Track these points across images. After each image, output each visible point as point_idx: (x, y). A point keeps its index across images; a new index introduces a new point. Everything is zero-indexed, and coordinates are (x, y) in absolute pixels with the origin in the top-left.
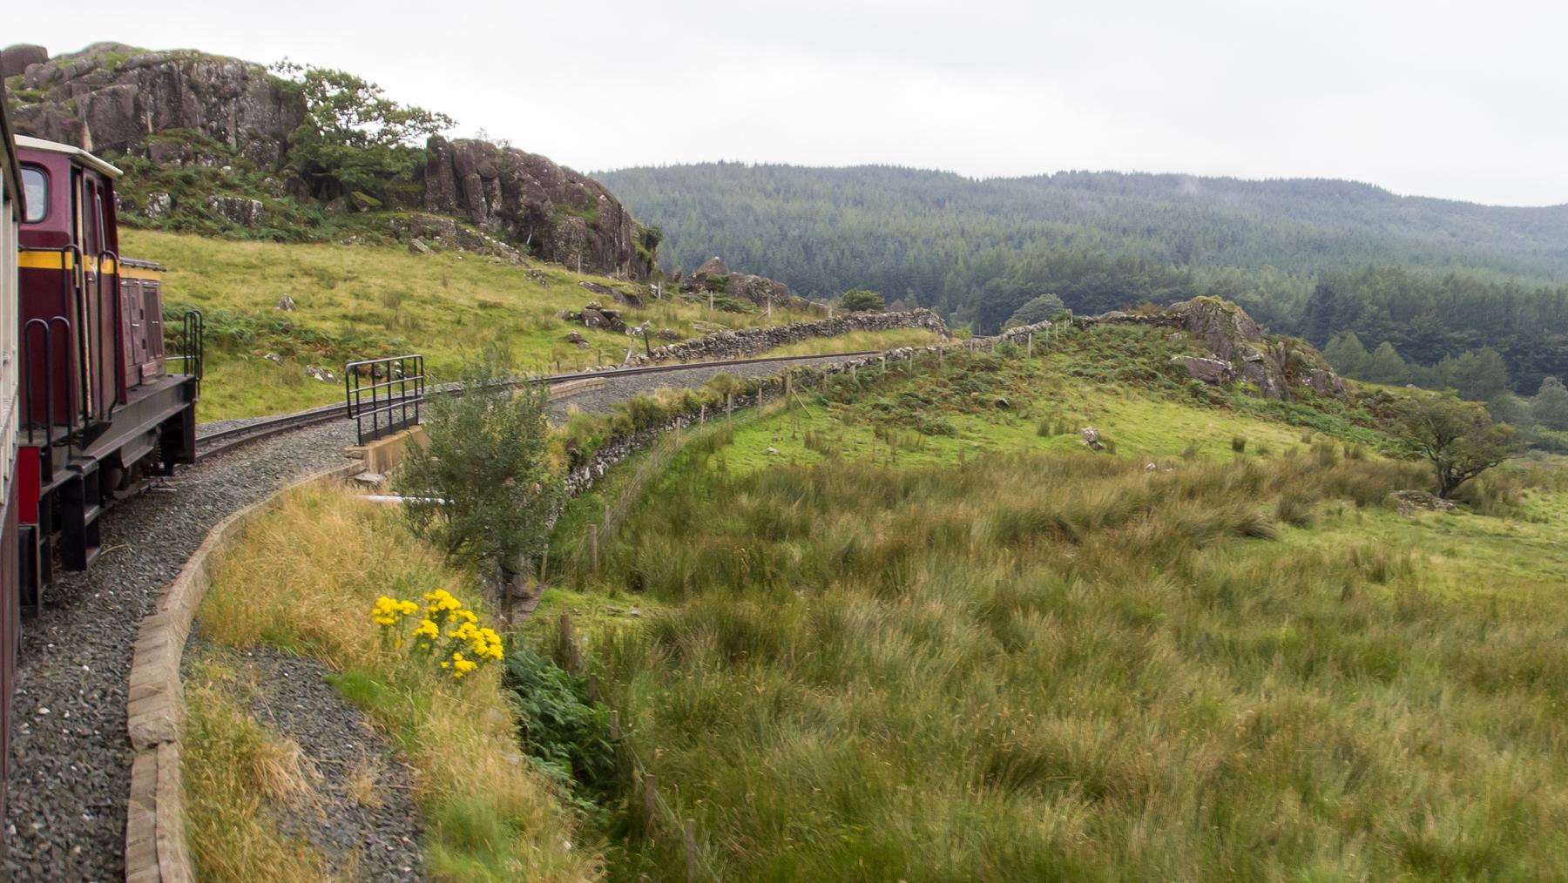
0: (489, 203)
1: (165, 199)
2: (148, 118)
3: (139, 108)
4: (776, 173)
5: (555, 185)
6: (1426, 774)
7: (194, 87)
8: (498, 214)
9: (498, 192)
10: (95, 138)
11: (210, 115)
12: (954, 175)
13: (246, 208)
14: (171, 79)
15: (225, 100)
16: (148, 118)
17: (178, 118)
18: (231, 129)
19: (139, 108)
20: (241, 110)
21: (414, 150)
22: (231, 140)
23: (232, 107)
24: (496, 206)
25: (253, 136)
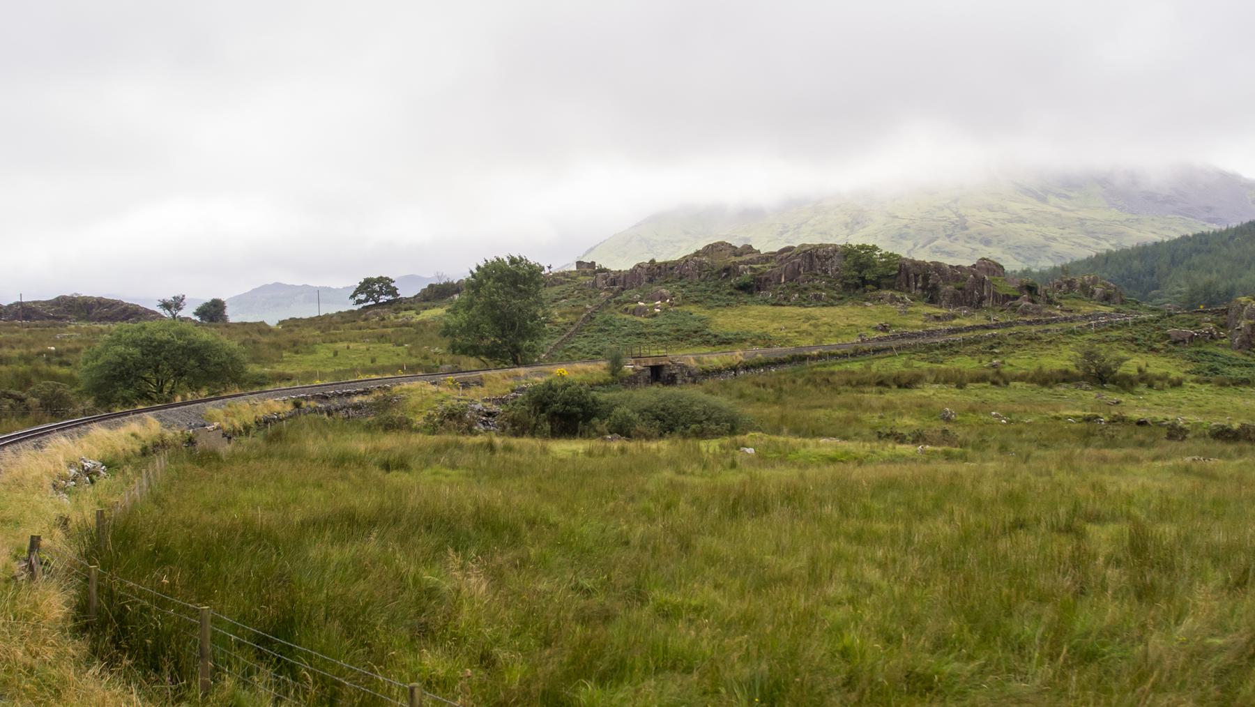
0: (916, 284)
1: (797, 295)
2: (801, 270)
3: (799, 266)
4: (663, 267)
5: (945, 274)
6: (1174, 533)
7: (817, 257)
8: (920, 288)
9: (920, 280)
10: (785, 278)
11: (822, 266)
12: (64, 298)
13: (820, 296)
14: (811, 255)
15: (827, 260)
16: (801, 270)
17: (811, 267)
18: (829, 269)
19: (799, 266)
20: (833, 262)
21: (570, 272)
22: (830, 272)
23: (830, 261)
24: (919, 285)
25: (837, 270)
